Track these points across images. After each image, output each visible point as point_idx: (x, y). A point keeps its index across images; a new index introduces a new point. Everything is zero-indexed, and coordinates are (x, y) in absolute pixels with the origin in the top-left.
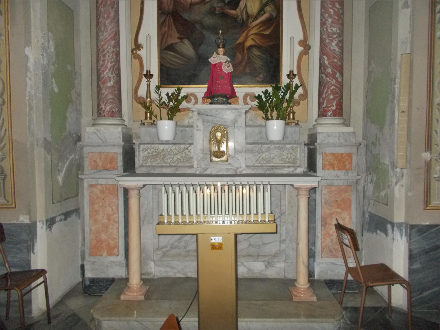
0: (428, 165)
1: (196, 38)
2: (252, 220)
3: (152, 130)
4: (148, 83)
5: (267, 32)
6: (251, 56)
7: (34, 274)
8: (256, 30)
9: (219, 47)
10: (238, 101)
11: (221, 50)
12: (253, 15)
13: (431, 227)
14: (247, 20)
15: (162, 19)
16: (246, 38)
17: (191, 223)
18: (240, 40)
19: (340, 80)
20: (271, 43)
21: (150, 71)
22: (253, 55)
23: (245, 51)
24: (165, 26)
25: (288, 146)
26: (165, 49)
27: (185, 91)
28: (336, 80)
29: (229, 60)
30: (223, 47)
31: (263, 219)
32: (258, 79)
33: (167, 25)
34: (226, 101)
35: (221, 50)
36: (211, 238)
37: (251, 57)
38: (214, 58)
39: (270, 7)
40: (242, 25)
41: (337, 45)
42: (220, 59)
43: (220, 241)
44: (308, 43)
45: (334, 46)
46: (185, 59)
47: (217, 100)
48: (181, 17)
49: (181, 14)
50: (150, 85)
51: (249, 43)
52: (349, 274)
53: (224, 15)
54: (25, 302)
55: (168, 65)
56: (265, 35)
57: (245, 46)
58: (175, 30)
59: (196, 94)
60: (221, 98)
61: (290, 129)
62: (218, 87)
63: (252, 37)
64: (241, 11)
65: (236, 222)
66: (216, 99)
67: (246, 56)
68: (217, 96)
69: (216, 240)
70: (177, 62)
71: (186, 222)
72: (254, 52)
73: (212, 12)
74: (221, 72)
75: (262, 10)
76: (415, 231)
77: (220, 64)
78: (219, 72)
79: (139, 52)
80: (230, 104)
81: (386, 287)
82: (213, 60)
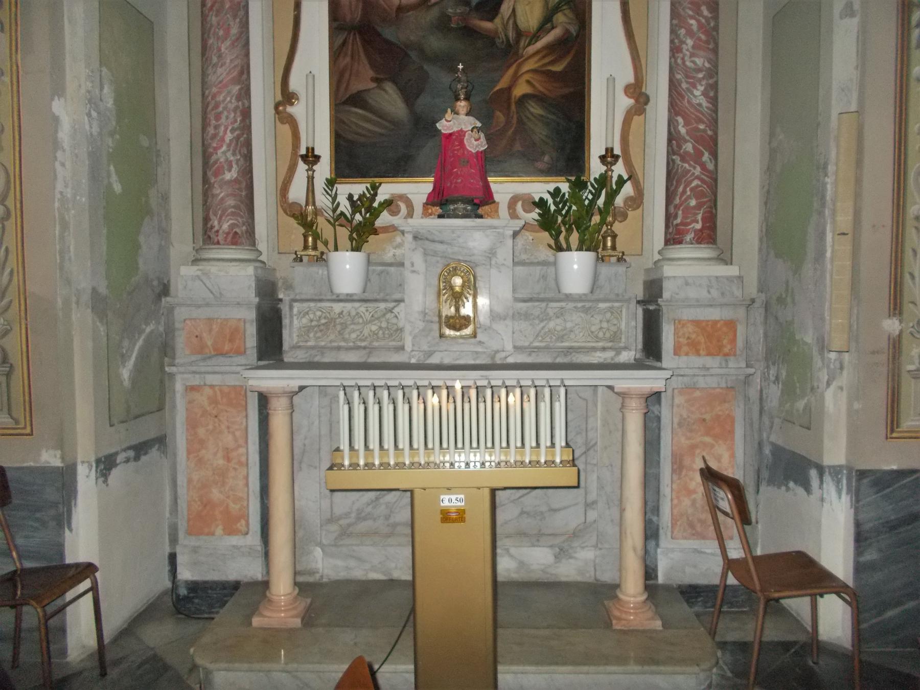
0: (896, 345)
1: (410, 80)
2: (527, 461)
3: (318, 271)
4: (310, 173)
5: (558, 68)
6: (524, 118)
7: (71, 573)
8: (536, 62)
9: (457, 99)
10: (497, 211)
11: (462, 105)
12: (530, 32)
13: (900, 474)
14: (517, 42)
15: (339, 41)
16: (515, 79)
17: (400, 465)
18: (503, 84)
19: (711, 166)
20: (566, 91)
21: (313, 149)
22: (530, 116)
23: (513, 107)
25: (602, 305)
26: (345, 103)
27: (387, 189)
28: (703, 166)
29: (479, 124)
30: (467, 98)
31: (550, 458)
32: (539, 165)
33: (349, 53)
34: (472, 211)
35: (462, 105)
36: (442, 497)
37: (526, 120)
38: (447, 121)
39: (565, 15)
40: (506, 52)
41: (704, 94)
42: (460, 124)
43: (459, 504)
44: (643, 90)
45: (698, 96)
46: (387, 124)
47: (454, 210)
48: (379, 35)
49: (379, 29)
51: (521, 89)
52: (730, 574)
53: (469, 32)
54: (53, 632)
55: (350, 137)
56: (555, 73)
57: (513, 97)
58: (366, 62)
59: (409, 196)
60: (462, 206)
61: (606, 270)
62: (456, 183)
63: (527, 77)
64: (503, 23)
65: (493, 464)
66: (452, 207)
67: (515, 116)
68: (455, 202)
69: (451, 501)
70: (369, 131)
71: (389, 465)
72: (532, 110)
73: (443, 25)
74: (461, 151)
76: (868, 483)
77: (461, 134)
78: (458, 150)
79: (290, 109)
80: (481, 217)
81: (807, 599)
82: (446, 125)
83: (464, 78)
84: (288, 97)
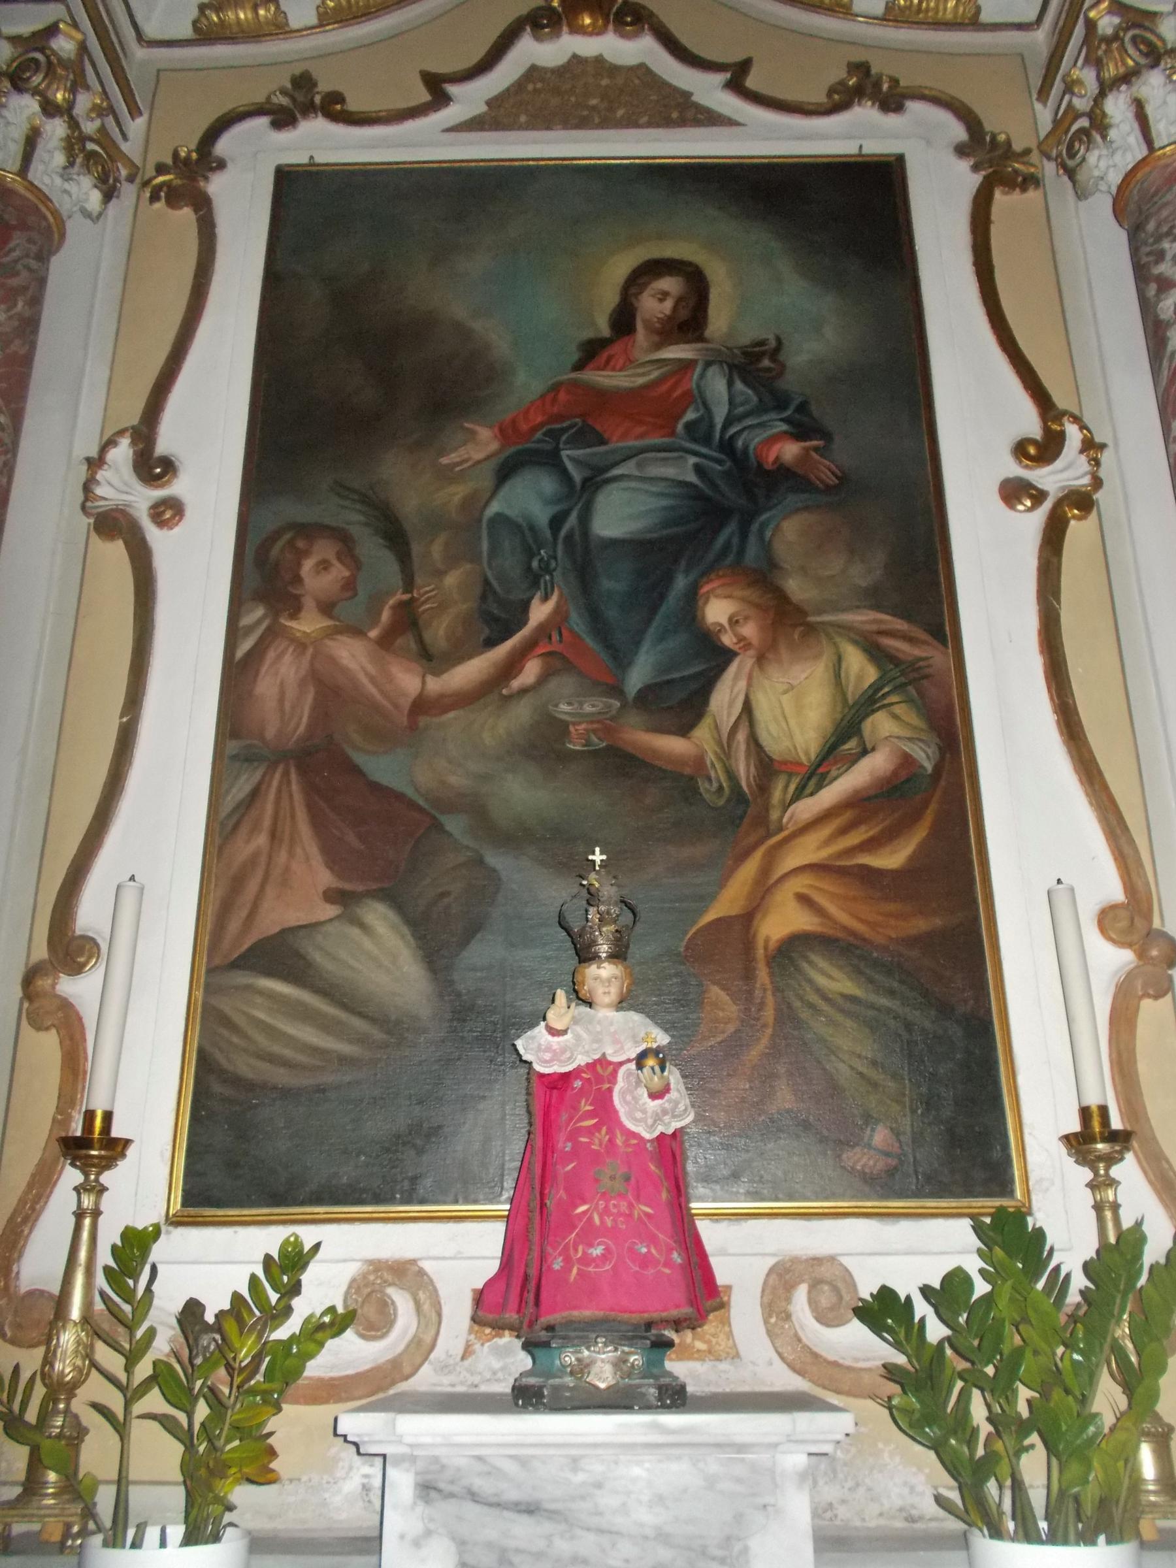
1: (443, 895)
4: (88, 1201)
5: (892, 859)
6: (797, 1004)
8: (828, 842)
9: (585, 954)
11: (604, 976)
12: (799, 764)
14: (763, 789)
15: (241, 788)
18: (727, 903)
20: (920, 925)
21: (108, 1116)
22: (814, 998)
23: (763, 974)
24: (255, 829)
26: (239, 964)
27: (343, 1249)
29: (661, 1038)
30: (618, 955)
32: (860, 1159)
33: (267, 823)
35: (604, 976)
37: (805, 1014)
38: (553, 1032)
39: (895, 717)
40: (738, 814)
44: (1156, 924)
48: (356, 771)
49: (359, 759)
50: (96, 1213)
51: (782, 920)
53: (619, 764)
55: (245, 1066)
56: (880, 872)
58: (313, 850)
59: (427, 1265)
62: (586, 1260)
63: (799, 884)
64: (719, 742)
67: (770, 1000)
68: (584, 1332)
70: (315, 1050)
72: (821, 981)
73: (545, 746)
74: (603, 1135)
75: (845, 737)
77: (600, 1073)
78: (590, 1131)
79: (67, 986)
82: (554, 1044)
83: (608, 891)
84: (69, 949)
